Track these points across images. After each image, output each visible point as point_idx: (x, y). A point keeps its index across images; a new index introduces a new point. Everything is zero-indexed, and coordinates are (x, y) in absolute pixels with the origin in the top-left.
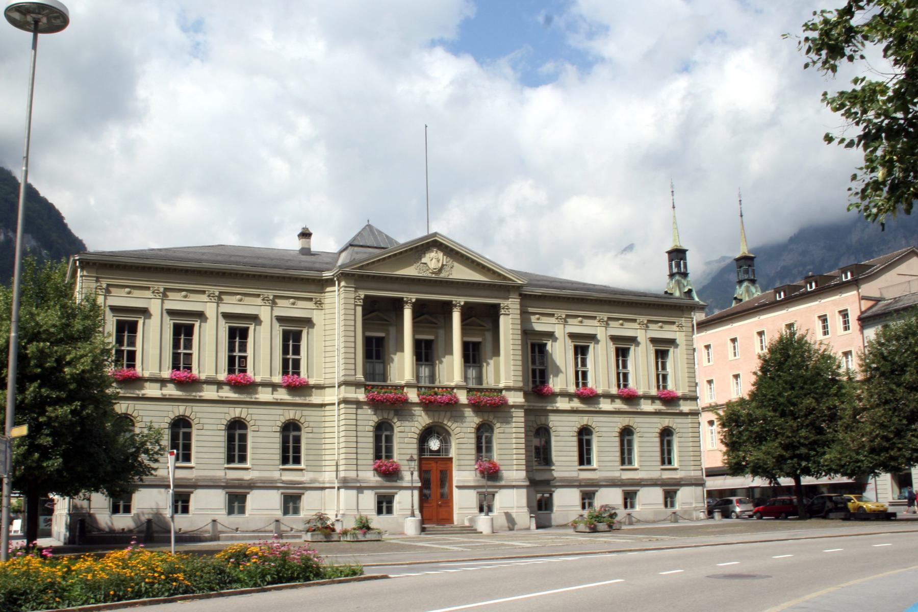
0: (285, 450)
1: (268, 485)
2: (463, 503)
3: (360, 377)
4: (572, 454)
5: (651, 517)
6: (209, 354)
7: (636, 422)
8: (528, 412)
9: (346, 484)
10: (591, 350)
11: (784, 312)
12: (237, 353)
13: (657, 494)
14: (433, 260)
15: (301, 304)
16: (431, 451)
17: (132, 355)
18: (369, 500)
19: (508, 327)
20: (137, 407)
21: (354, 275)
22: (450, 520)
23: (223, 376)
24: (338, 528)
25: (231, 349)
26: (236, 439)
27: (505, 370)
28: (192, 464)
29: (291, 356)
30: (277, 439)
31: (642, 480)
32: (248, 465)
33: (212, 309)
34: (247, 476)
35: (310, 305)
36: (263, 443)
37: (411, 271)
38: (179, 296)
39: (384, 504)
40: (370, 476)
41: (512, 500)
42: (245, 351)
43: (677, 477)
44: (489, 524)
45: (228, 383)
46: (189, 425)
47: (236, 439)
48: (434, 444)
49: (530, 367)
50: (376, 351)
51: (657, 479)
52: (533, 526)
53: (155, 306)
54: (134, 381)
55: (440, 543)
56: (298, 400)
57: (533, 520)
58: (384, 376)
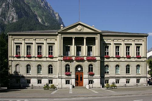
0: (49, 71)
1: (45, 78)
2: (85, 81)
3: (62, 55)
4: (87, 69)
5: (133, 85)
6: (122, 52)
7: (130, 63)
8: (101, 62)
9: (59, 78)
10: (120, 47)
11: (112, 31)
12: (128, 52)
13: (135, 80)
14: (79, 28)
15: (52, 40)
16: (78, 71)
17: (52, 53)
18: (64, 81)
19: (97, 42)
20: (120, 63)
21: (60, 32)
22: (82, 85)
23: (125, 56)
24: (57, 87)
25: (38, 50)
26: (39, 67)
27: (96, 51)
28: (109, 74)
29: (128, 52)
30: (47, 68)
31: (131, 77)
32: (130, 74)
33: (123, 43)
34: (41, 76)
35: (54, 40)
36: (45, 69)
37: (73, 30)
38: (27, 40)
39: (68, 82)
40: (64, 76)
41: (97, 82)
42: (52, 51)
43: (120, 76)
44: (89, 86)
45: (49, 57)
46: (52, 66)
47: (39, 67)
48: (79, 69)
49: (53, 51)
50: (66, 49)
51: (135, 77)
52: (101, 87)
53: (123, 43)
54: (109, 58)
55: (78, 90)
56: (119, 60)
57: (101, 86)
58: (68, 55)
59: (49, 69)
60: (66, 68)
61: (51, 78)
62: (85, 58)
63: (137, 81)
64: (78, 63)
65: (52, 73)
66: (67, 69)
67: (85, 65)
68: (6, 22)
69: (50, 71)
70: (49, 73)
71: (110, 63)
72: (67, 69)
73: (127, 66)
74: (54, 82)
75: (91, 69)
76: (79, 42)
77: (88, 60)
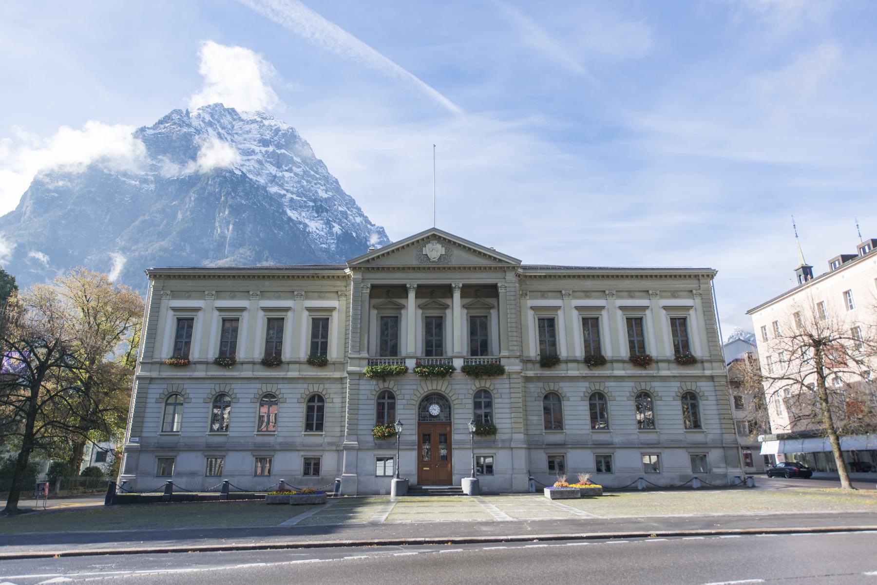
1: (580, 445)
16: (431, 416)
29: (434, 338)
48: (435, 410)
59: (310, 409)
60: (380, 407)
61: (696, 445)
62: (458, 363)
63: (598, 463)
64: (429, 384)
65: (322, 430)
66: (385, 409)
67: (461, 391)
68: (300, 214)
69: (315, 418)
70: (309, 427)
71: (611, 384)
72: (385, 409)
73: (311, 399)
74: (328, 463)
75: (483, 402)
76: (435, 295)
77: (470, 371)
